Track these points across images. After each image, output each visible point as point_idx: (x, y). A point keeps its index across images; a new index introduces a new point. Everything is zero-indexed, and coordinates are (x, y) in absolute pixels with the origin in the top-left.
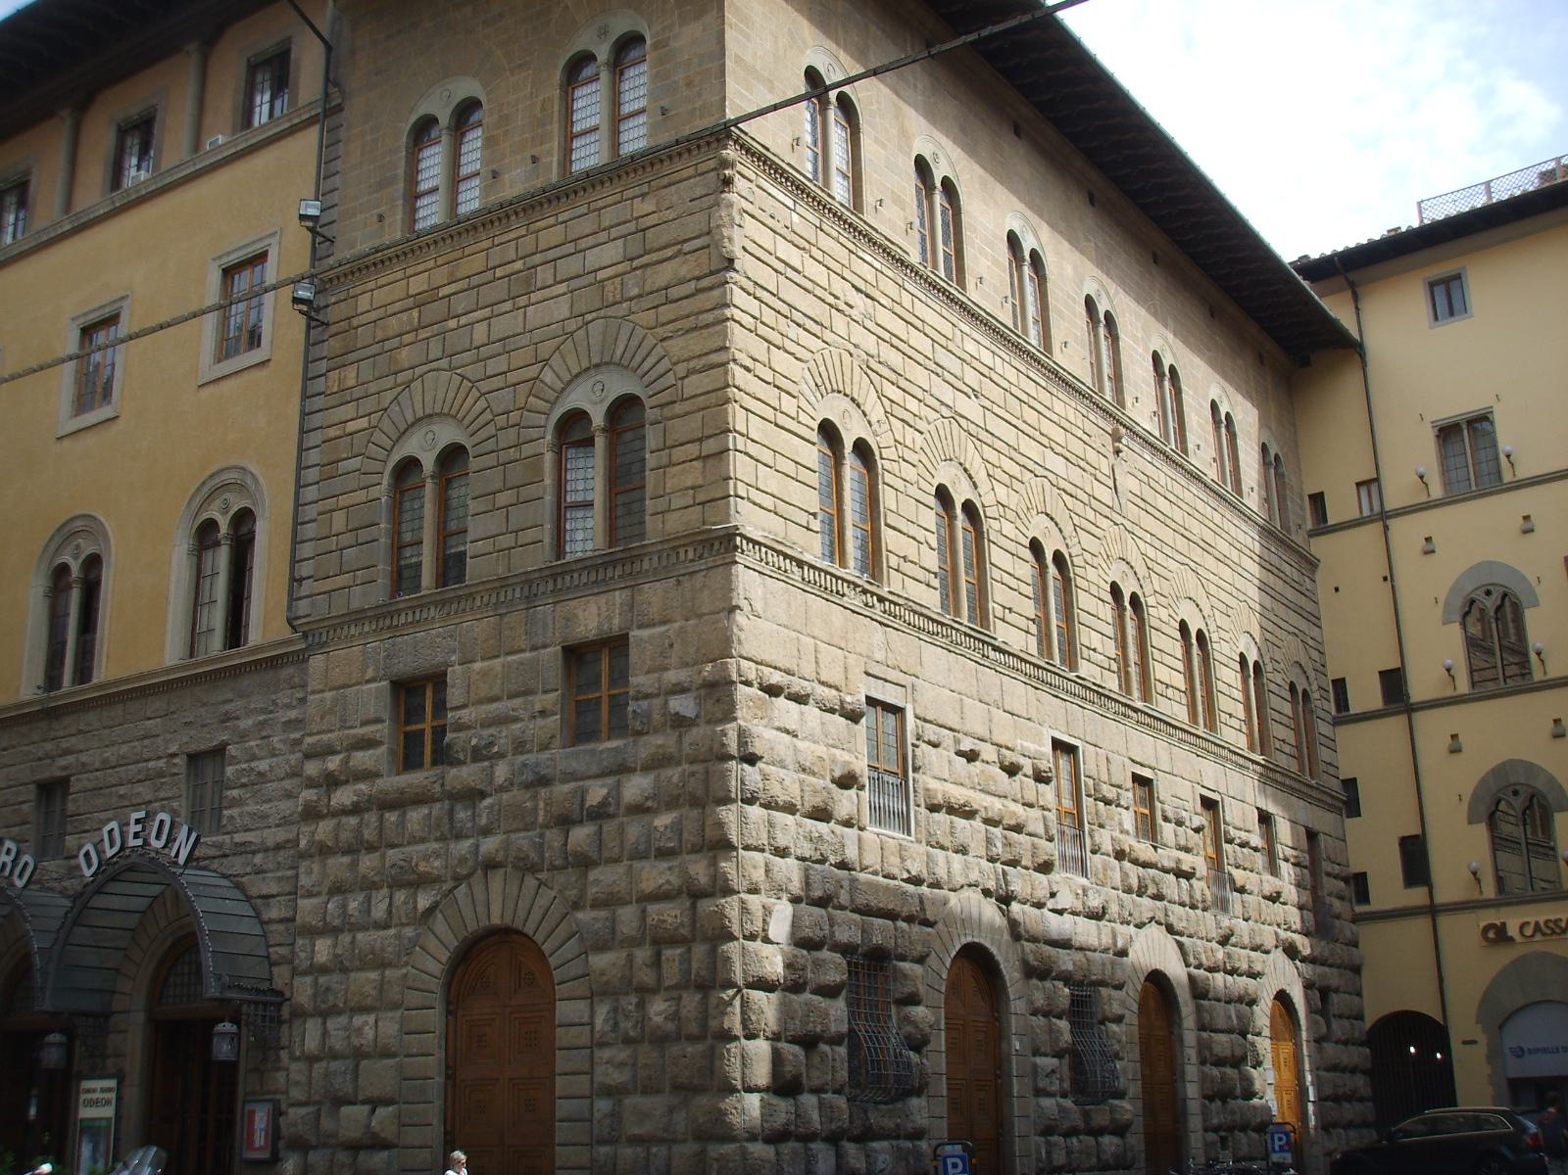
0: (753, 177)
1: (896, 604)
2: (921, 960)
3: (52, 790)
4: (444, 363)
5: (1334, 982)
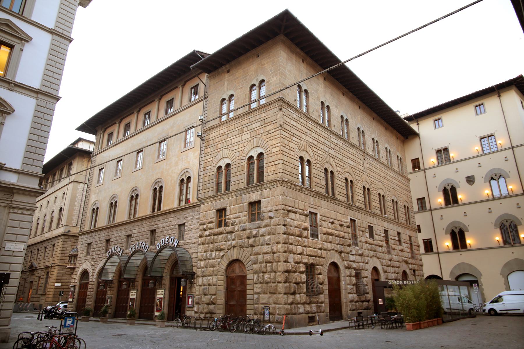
2: (322, 265)
3: (153, 232)
4: (226, 147)
5: (416, 268)
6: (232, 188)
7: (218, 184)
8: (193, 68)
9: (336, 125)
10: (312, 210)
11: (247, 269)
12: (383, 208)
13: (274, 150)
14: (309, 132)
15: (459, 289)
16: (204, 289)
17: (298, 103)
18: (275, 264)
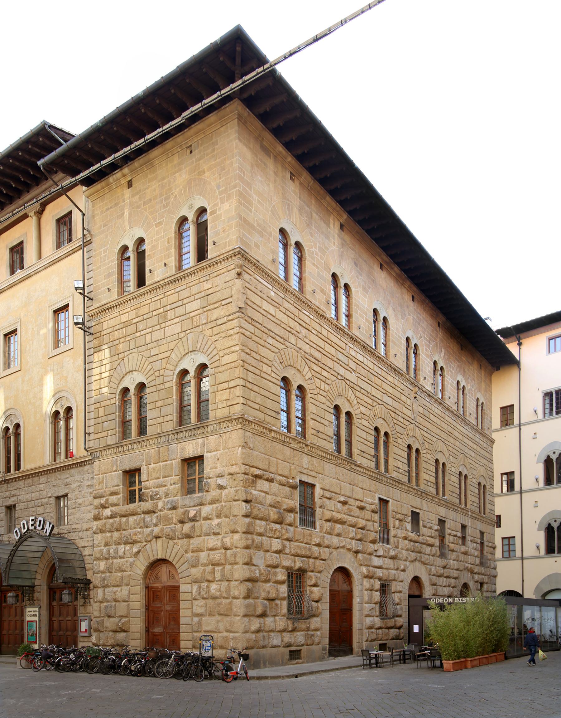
0: (252, 273)
1: (313, 447)
2: (320, 572)
3: (10, 508)
6: (150, 430)
7: (125, 424)
8: (45, 165)
9: (363, 326)
10: (305, 479)
11: (180, 576)
12: (440, 485)
13: (226, 359)
14: (304, 332)
15: (540, 611)
16: (106, 607)
17: (333, 308)
18: (228, 567)
